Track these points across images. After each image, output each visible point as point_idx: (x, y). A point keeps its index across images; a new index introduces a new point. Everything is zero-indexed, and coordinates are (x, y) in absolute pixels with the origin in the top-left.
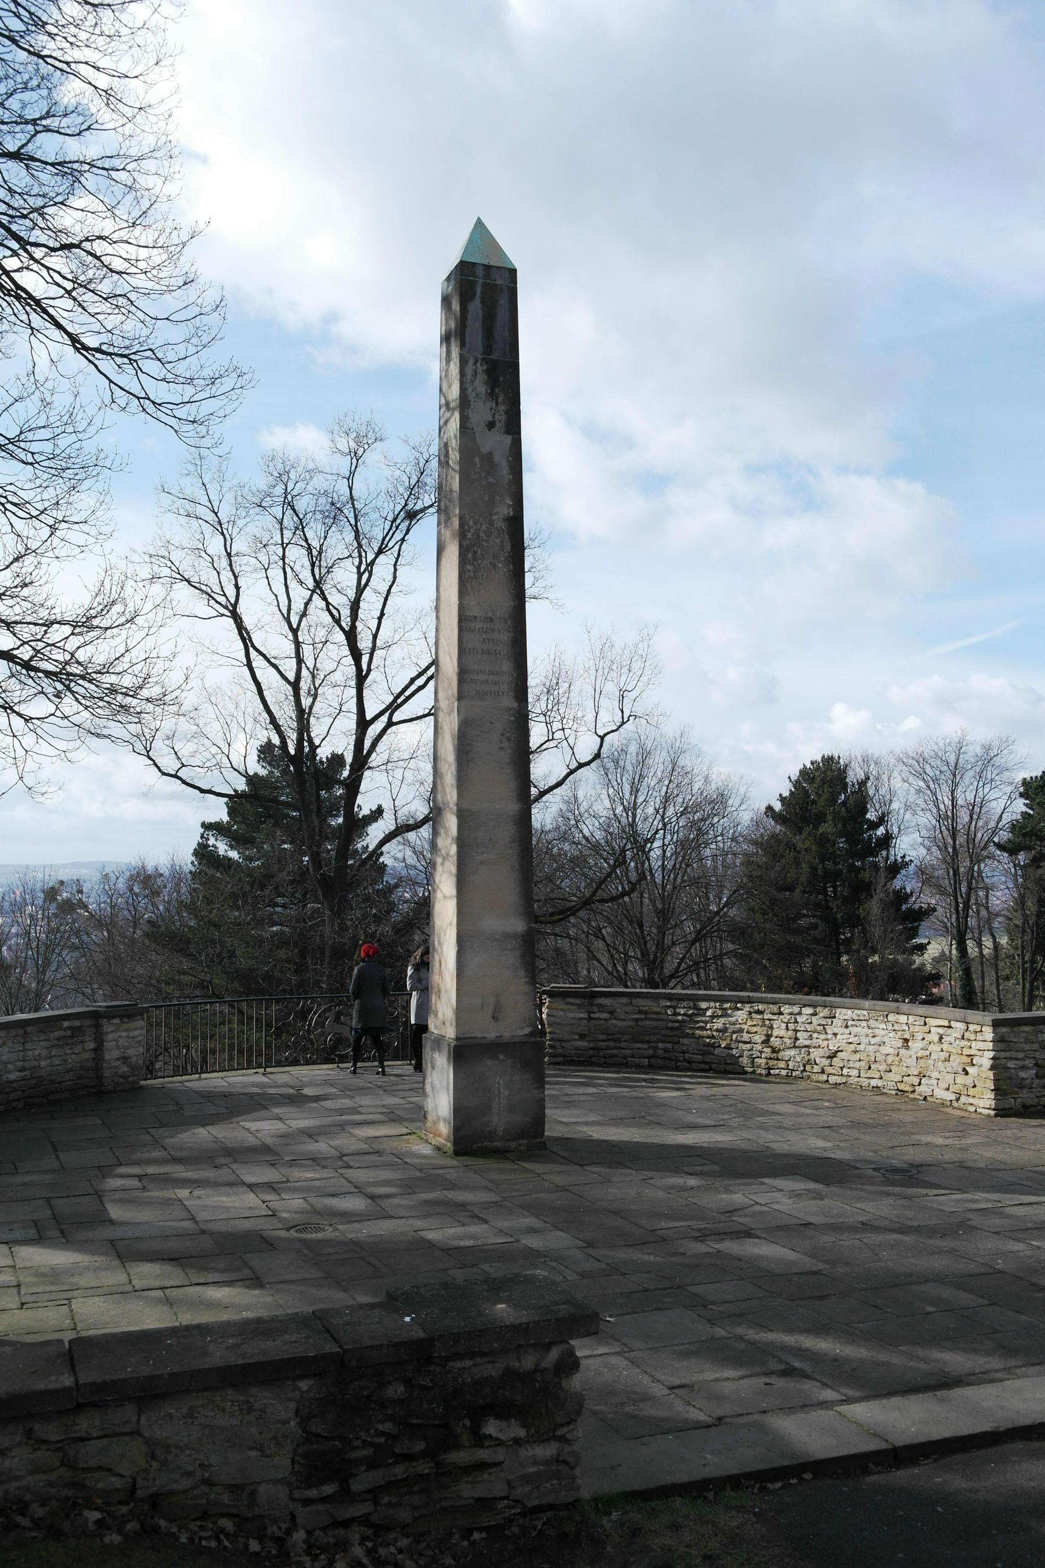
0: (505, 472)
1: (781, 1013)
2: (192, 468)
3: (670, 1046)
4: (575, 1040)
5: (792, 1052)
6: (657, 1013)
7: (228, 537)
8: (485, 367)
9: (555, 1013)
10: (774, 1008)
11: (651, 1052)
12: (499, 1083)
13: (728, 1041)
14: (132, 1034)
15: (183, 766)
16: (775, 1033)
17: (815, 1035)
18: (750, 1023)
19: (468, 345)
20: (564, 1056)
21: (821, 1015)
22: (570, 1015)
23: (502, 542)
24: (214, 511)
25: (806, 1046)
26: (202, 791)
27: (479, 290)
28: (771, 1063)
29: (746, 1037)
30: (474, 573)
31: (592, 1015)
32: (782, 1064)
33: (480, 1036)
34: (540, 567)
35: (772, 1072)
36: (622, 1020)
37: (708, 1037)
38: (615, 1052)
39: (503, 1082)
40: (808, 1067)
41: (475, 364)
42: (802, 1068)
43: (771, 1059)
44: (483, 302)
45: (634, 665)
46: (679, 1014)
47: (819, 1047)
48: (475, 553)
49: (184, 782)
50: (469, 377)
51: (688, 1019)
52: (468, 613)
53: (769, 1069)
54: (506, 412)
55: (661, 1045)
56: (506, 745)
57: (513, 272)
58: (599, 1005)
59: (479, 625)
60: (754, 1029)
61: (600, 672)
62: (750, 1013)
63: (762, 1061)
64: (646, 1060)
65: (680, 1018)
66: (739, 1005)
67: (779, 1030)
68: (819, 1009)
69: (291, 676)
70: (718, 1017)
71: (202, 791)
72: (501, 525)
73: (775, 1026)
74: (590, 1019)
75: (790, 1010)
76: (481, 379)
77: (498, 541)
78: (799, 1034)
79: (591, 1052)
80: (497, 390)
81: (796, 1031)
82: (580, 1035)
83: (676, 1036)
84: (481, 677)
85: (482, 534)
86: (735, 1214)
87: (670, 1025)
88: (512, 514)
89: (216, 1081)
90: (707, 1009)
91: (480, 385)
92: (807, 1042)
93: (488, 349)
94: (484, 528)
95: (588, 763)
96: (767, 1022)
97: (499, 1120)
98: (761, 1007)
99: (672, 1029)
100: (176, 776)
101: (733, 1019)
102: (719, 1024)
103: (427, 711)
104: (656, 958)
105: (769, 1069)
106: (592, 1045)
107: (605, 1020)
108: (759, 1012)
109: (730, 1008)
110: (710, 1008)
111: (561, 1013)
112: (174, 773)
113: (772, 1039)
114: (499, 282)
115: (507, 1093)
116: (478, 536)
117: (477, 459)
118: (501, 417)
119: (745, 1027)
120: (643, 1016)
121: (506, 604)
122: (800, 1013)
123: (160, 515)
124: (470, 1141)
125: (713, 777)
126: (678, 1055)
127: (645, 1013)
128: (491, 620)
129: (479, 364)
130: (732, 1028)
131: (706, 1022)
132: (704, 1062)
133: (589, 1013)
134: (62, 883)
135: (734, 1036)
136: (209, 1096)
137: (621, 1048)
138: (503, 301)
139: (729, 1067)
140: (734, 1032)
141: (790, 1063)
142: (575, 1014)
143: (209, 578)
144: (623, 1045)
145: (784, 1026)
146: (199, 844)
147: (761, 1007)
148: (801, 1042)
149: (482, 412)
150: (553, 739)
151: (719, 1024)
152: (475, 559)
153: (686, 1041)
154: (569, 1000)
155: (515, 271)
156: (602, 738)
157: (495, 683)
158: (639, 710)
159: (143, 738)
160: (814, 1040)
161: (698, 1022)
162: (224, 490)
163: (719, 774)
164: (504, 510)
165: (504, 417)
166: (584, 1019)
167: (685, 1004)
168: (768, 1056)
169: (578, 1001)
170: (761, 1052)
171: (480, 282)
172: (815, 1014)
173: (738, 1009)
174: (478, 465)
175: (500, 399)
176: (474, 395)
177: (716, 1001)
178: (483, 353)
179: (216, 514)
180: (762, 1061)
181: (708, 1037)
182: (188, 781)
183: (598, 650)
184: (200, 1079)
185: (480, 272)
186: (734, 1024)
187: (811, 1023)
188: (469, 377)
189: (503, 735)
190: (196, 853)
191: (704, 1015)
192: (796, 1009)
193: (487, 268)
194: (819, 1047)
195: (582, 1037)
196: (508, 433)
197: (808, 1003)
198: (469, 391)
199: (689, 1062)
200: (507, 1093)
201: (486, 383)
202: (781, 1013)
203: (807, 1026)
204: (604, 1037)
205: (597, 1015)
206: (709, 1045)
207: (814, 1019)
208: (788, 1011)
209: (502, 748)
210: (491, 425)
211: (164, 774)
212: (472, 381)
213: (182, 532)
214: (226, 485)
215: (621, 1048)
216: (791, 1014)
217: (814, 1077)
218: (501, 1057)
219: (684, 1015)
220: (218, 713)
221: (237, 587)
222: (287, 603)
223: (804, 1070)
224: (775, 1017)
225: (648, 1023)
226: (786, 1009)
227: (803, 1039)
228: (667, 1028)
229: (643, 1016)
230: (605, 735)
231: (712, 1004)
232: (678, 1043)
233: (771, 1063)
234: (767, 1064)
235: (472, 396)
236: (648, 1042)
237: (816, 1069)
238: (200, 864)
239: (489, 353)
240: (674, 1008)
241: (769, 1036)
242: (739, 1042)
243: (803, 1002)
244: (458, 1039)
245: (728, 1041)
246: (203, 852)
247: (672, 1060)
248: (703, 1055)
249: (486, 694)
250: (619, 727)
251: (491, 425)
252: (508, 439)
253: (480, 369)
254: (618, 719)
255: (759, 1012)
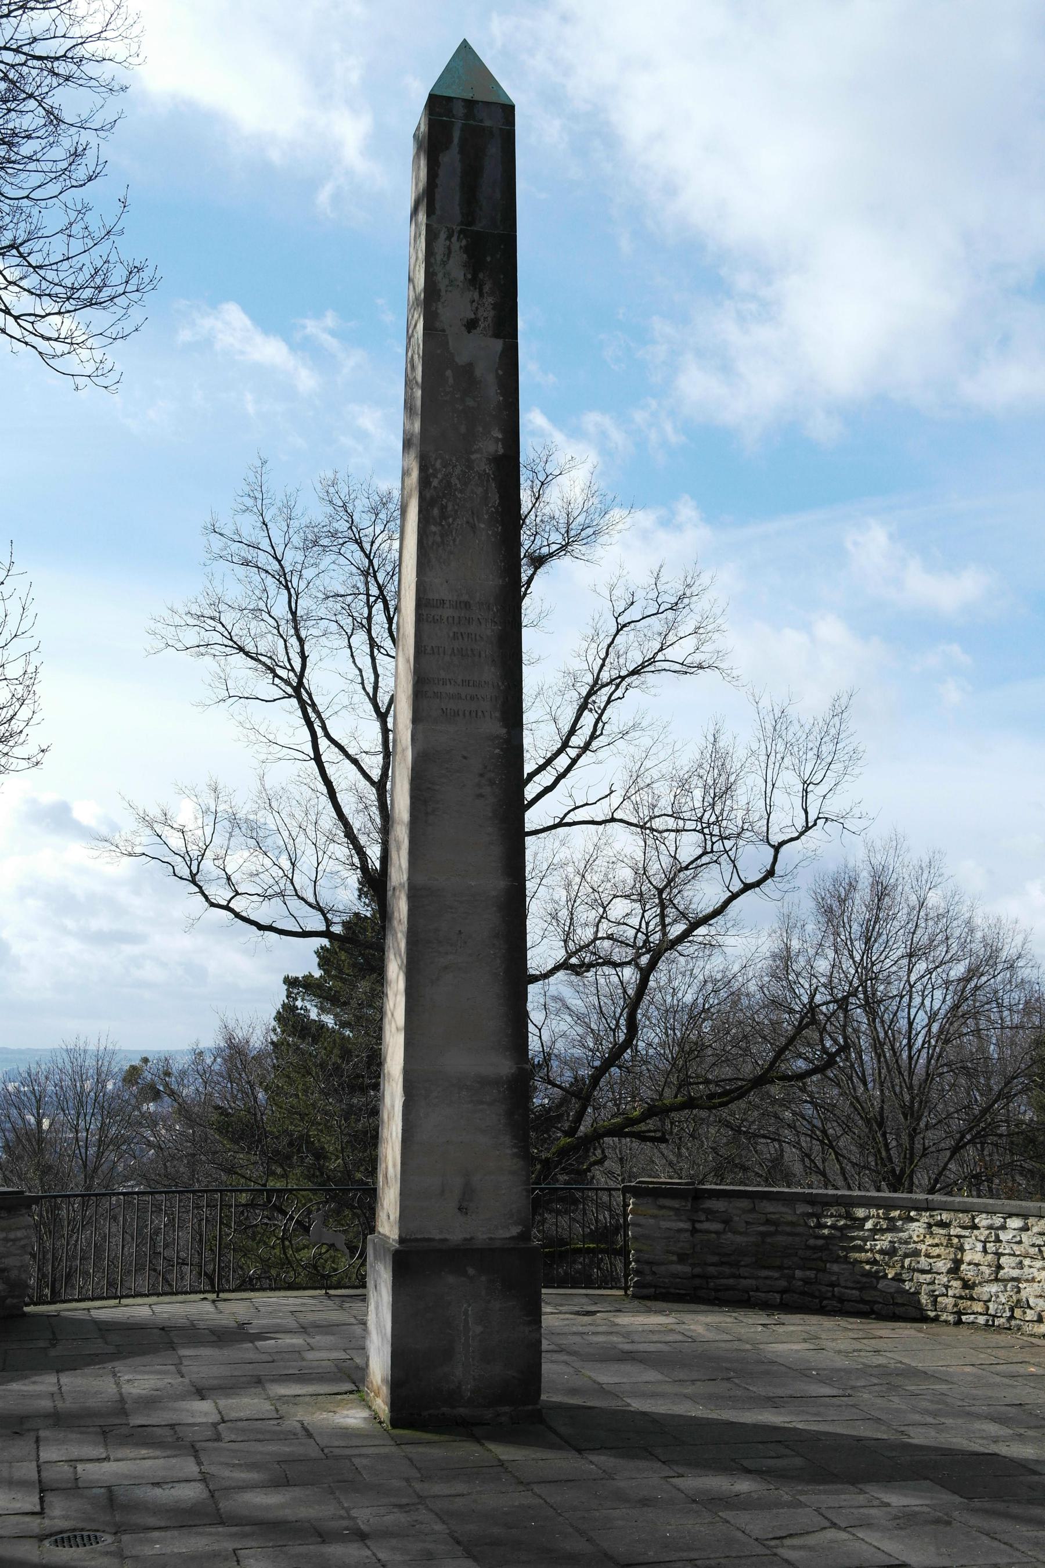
0: (493, 393)
1: (975, 1227)
2: (250, 502)
3: (811, 1274)
4: (672, 1262)
5: (994, 1288)
6: (792, 1224)
7: (292, 591)
8: (464, 242)
9: (642, 1220)
10: (965, 1218)
11: (783, 1283)
12: (466, 1313)
13: (898, 1269)
14: (12, 1235)
15: (237, 894)
16: (968, 1257)
17: (1027, 1262)
18: (929, 1241)
19: (438, 212)
20: (656, 1287)
21: (1035, 1229)
22: (664, 1224)
23: (486, 492)
24: (276, 558)
25: (1013, 1279)
26: (261, 927)
27: (456, 135)
28: (963, 1304)
29: (924, 1262)
30: (442, 536)
31: (698, 1226)
32: (978, 1307)
33: (438, 1237)
34: (709, 628)
35: (964, 1318)
36: (741, 1233)
37: (868, 1262)
38: (731, 1281)
39: (471, 1310)
40: (1018, 1313)
41: (449, 238)
42: (1008, 1314)
43: (961, 1297)
44: (462, 151)
45: (824, 748)
46: (825, 1227)
47: (1033, 1280)
48: (443, 509)
49: (237, 915)
50: (439, 258)
51: (838, 1234)
52: (430, 596)
53: (959, 1313)
54: (495, 306)
55: (798, 1273)
56: (487, 790)
57: (509, 110)
58: (709, 1212)
59: (448, 612)
60: (936, 1251)
61: (772, 758)
62: (930, 1226)
63: (948, 1302)
64: (778, 1296)
65: (826, 1232)
66: (912, 1214)
67: (973, 1254)
68: (1031, 1221)
69: (376, 774)
70: (883, 1231)
71: (261, 927)
72: (483, 466)
73: (967, 1247)
74: (694, 1231)
75: (989, 1222)
76: (458, 258)
77: (480, 490)
78: (1003, 1260)
79: (697, 1282)
80: (481, 275)
81: (998, 1255)
82: (678, 1255)
83: (821, 1259)
84: (450, 689)
85: (454, 480)
86: (788, 1542)
87: (812, 1242)
88: (501, 451)
89: (139, 1310)
90: (866, 1219)
91: (456, 268)
92: (1015, 1273)
93: (469, 217)
94: (458, 471)
95: (758, 884)
96: (955, 1241)
97: (465, 1372)
98: (945, 1216)
99: (814, 1248)
100: (227, 908)
101: (904, 1235)
102: (883, 1242)
103: (557, 820)
104: (903, 1171)
105: (959, 1313)
106: (698, 1270)
107: (716, 1233)
108: (942, 1224)
109: (900, 1218)
110: (870, 1218)
111: (652, 1221)
112: (225, 903)
113: (963, 1267)
114: (488, 123)
115: (479, 1329)
116: (449, 484)
117: (449, 373)
118: (487, 314)
119: (923, 1247)
120: (772, 1229)
121: (487, 581)
122: (1003, 1227)
123: (209, 562)
124: (419, 1404)
125: (978, 921)
126: (824, 1289)
127: (775, 1223)
128: (467, 605)
129: (454, 239)
130: (903, 1249)
131: (865, 1240)
132: (862, 1301)
133: (693, 1222)
134: (146, 1060)
135: (907, 1261)
136: (104, 1328)
137: (740, 1277)
138: (494, 150)
139: (904, 1309)
140: (906, 1256)
141: (991, 1305)
142: (670, 1223)
143: (268, 644)
144: (743, 1271)
145: (979, 1246)
146: (284, 1005)
147: (945, 1216)
148: (1007, 1272)
149: (458, 305)
150: (712, 851)
151: (883, 1242)
152: (443, 516)
153: (835, 1268)
154: (663, 1201)
155: (512, 107)
156: (777, 849)
157: (472, 698)
158: (832, 807)
159: (187, 858)
160: (1026, 1270)
161: (854, 1238)
162: (291, 531)
163: (986, 918)
164: (491, 445)
165: (492, 313)
166: (686, 1230)
167: (833, 1210)
168: (958, 1292)
169: (676, 1204)
170: (947, 1287)
171: (458, 124)
172: (1025, 1229)
173: (913, 1220)
174: (451, 381)
175: (487, 288)
176: (446, 282)
177: (878, 1207)
178: (462, 223)
179: (279, 562)
180: (948, 1302)
181: (868, 1262)
182: (244, 914)
183: (769, 727)
184: (119, 1305)
185: (459, 110)
186: (906, 1243)
187: (1020, 1242)
188: (439, 258)
189: (481, 775)
190: (279, 1017)
191: (861, 1228)
192: (998, 1221)
193: (470, 104)
194: (1033, 1280)
195: (682, 1258)
196: (497, 336)
197: (1014, 1211)
198: (440, 276)
199: (841, 1300)
200: (479, 1329)
201: (465, 265)
202: (975, 1227)
203: (1015, 1247)
204: (715, 1259)
205: (706, 1226)
206: (868, 1274)
207: (1025, 1237)
208: (985, 1223)
209: (480, 796)
210: (471, 325)
211: (212, 905)
212: (444, 263)
213: (236, 587)
214: (295, 524)
215: (740, 1277)
216: (990, 1227)
217: (1028, 1328)
218: (471, 1271)
219: (833, 1227)
220: (280, 822)
221: (304, 658)
222: (372, 680)
223: (1012, 1317)
224: (966, 1233)
225: (780, 1238)
226: (982, 1220)
227: (1009, 1271)
228: (808, 1247)
229: (772, 1229)
230: (782, 844)
231: (873, 1211)
232: (824, 1270)
233: (963, 1304)
234: (956, 1305)
235: (442, 284)
236: (780, 1268)
237: (1030, 1315)
238: (283, 1032)
239: (471, 224)
240: (818, 1216)
241: (958, 1263)
242: (914, 1270)
243: (1007, 1209)
244: (402, 1240)
245: (898, 1269)
246: (288, 1018)
247: (816, 1297)
248: (860, 1289)
249: (456, 714)
250: (802, 833)
251: (471, 325)
252: (498, 345)
253: (456, 245)
254: (800, 824)
255: (942, 1224)
